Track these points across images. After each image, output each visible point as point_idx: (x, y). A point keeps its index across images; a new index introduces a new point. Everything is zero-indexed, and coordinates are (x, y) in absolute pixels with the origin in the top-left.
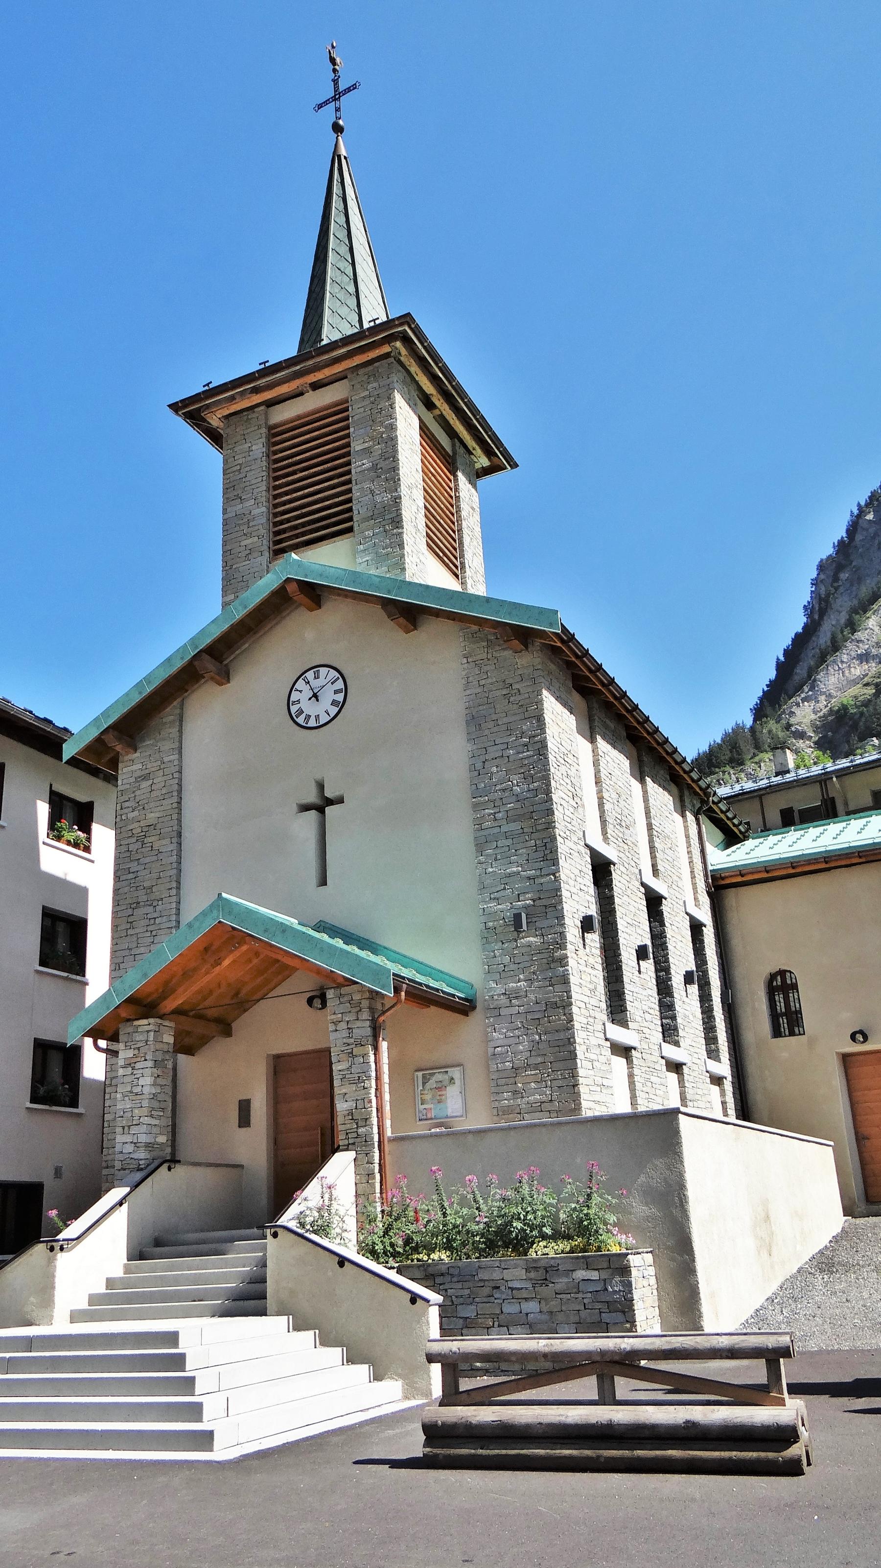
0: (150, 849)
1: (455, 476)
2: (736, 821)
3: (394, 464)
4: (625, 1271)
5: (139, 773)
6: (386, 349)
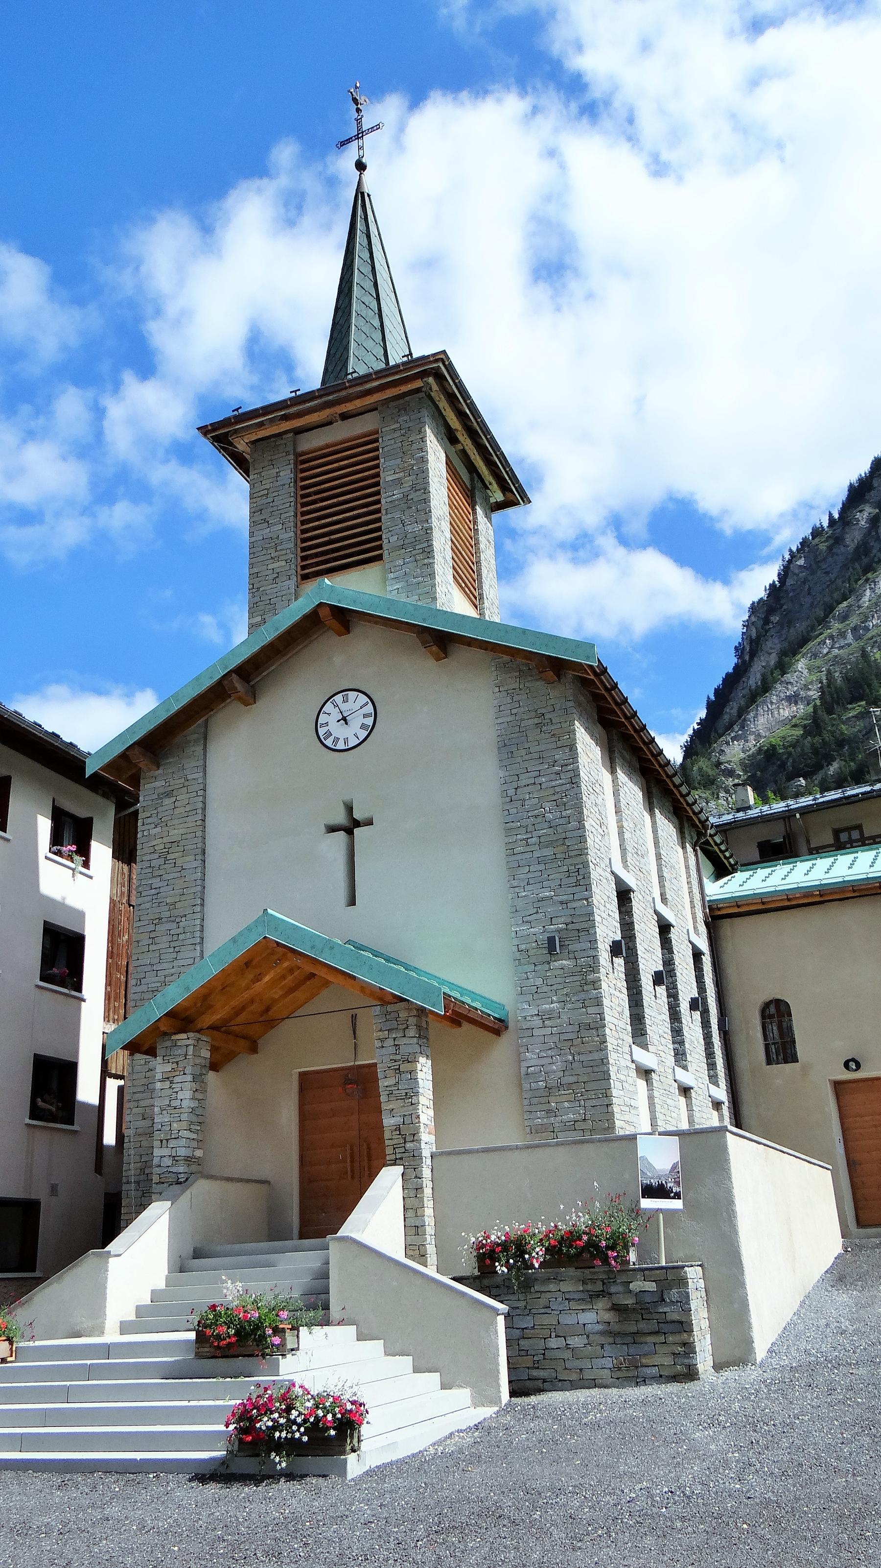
0: (173, 865)
1: (474, 510)
2: (727, 854)
3: (424, 496)
4: (682, 1282)
5: (162, 790)
6: (418, 384)
